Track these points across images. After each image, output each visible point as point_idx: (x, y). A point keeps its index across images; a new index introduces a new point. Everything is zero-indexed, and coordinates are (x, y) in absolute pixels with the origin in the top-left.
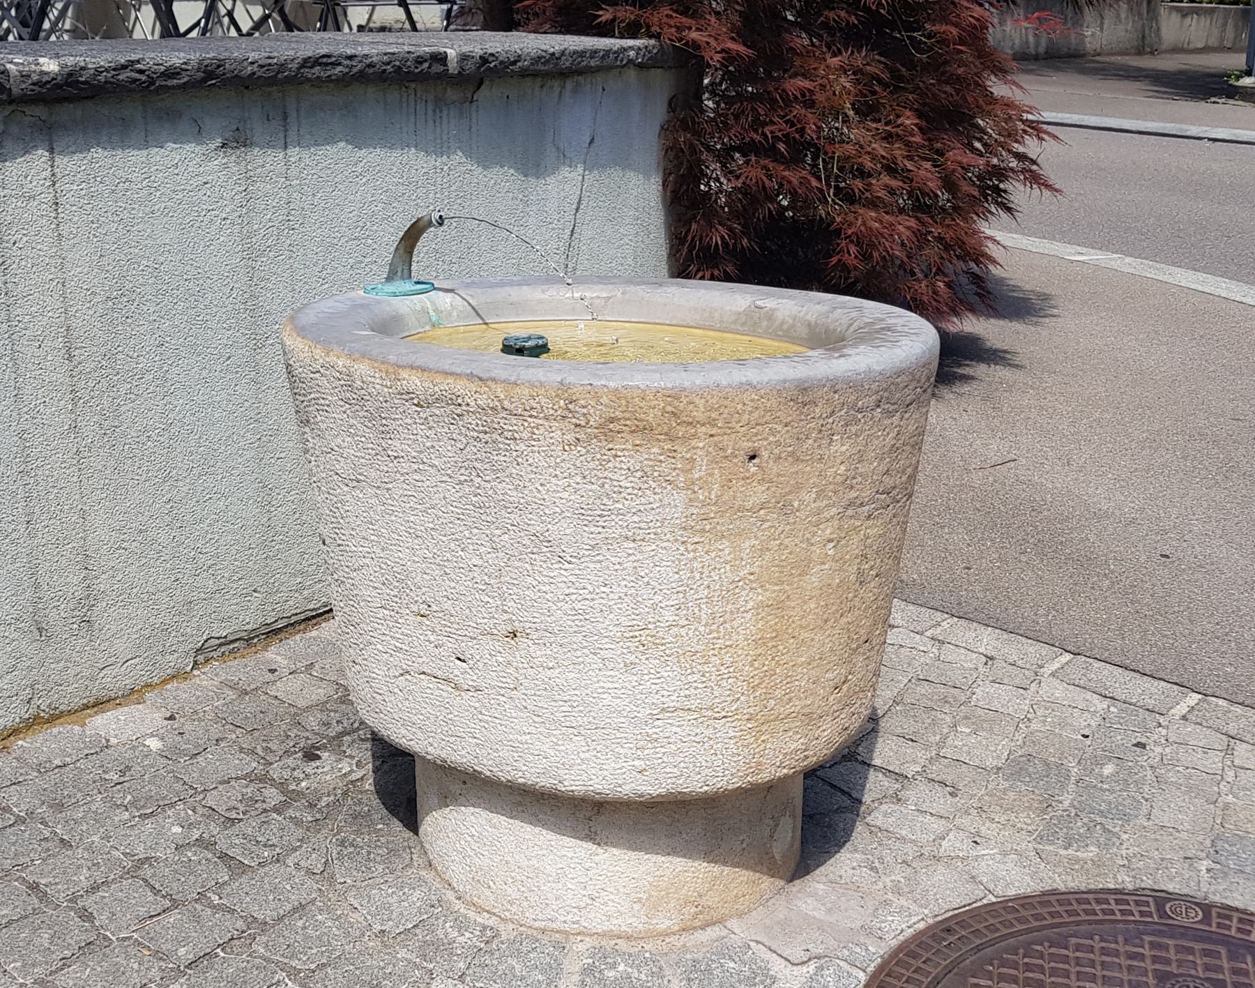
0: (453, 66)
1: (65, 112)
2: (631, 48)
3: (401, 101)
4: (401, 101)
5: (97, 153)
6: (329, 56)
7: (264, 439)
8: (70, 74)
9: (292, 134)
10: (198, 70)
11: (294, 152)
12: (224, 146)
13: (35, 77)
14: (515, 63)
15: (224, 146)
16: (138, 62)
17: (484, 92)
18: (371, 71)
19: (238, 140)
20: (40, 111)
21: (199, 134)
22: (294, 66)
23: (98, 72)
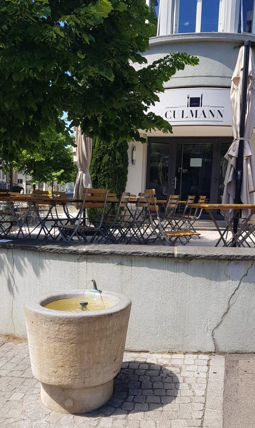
0: (176, 256)
1: (89, 256)
2: (6, 186)
3: (163, 261)
4: (163, 261)
5: (94, 263)
6: (239, 256)
7: (160, 299)
8: (87, 251)
9: (133, 264)
10: (110, 252)
11: (133, 267)
12: (118, 264)
13: (82, 251)
14: (199, 256)
15: (118, 264)
16: (100, 250)
17: (192, 262)
18: (150, 255)
19: (121, 264)
20: (85, 256)
21: (113, 262)
22: (130, 253)
23: (92, 251)
